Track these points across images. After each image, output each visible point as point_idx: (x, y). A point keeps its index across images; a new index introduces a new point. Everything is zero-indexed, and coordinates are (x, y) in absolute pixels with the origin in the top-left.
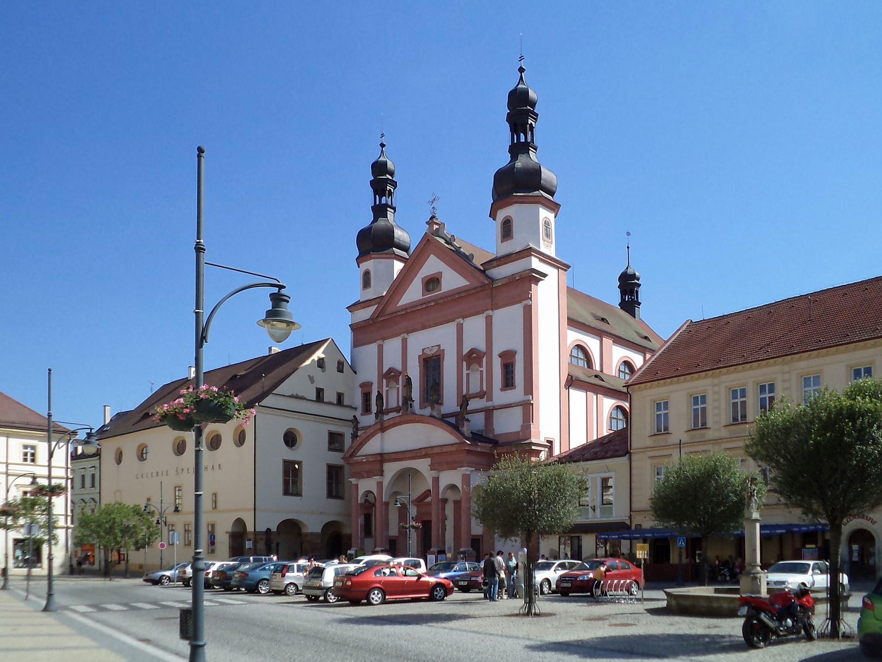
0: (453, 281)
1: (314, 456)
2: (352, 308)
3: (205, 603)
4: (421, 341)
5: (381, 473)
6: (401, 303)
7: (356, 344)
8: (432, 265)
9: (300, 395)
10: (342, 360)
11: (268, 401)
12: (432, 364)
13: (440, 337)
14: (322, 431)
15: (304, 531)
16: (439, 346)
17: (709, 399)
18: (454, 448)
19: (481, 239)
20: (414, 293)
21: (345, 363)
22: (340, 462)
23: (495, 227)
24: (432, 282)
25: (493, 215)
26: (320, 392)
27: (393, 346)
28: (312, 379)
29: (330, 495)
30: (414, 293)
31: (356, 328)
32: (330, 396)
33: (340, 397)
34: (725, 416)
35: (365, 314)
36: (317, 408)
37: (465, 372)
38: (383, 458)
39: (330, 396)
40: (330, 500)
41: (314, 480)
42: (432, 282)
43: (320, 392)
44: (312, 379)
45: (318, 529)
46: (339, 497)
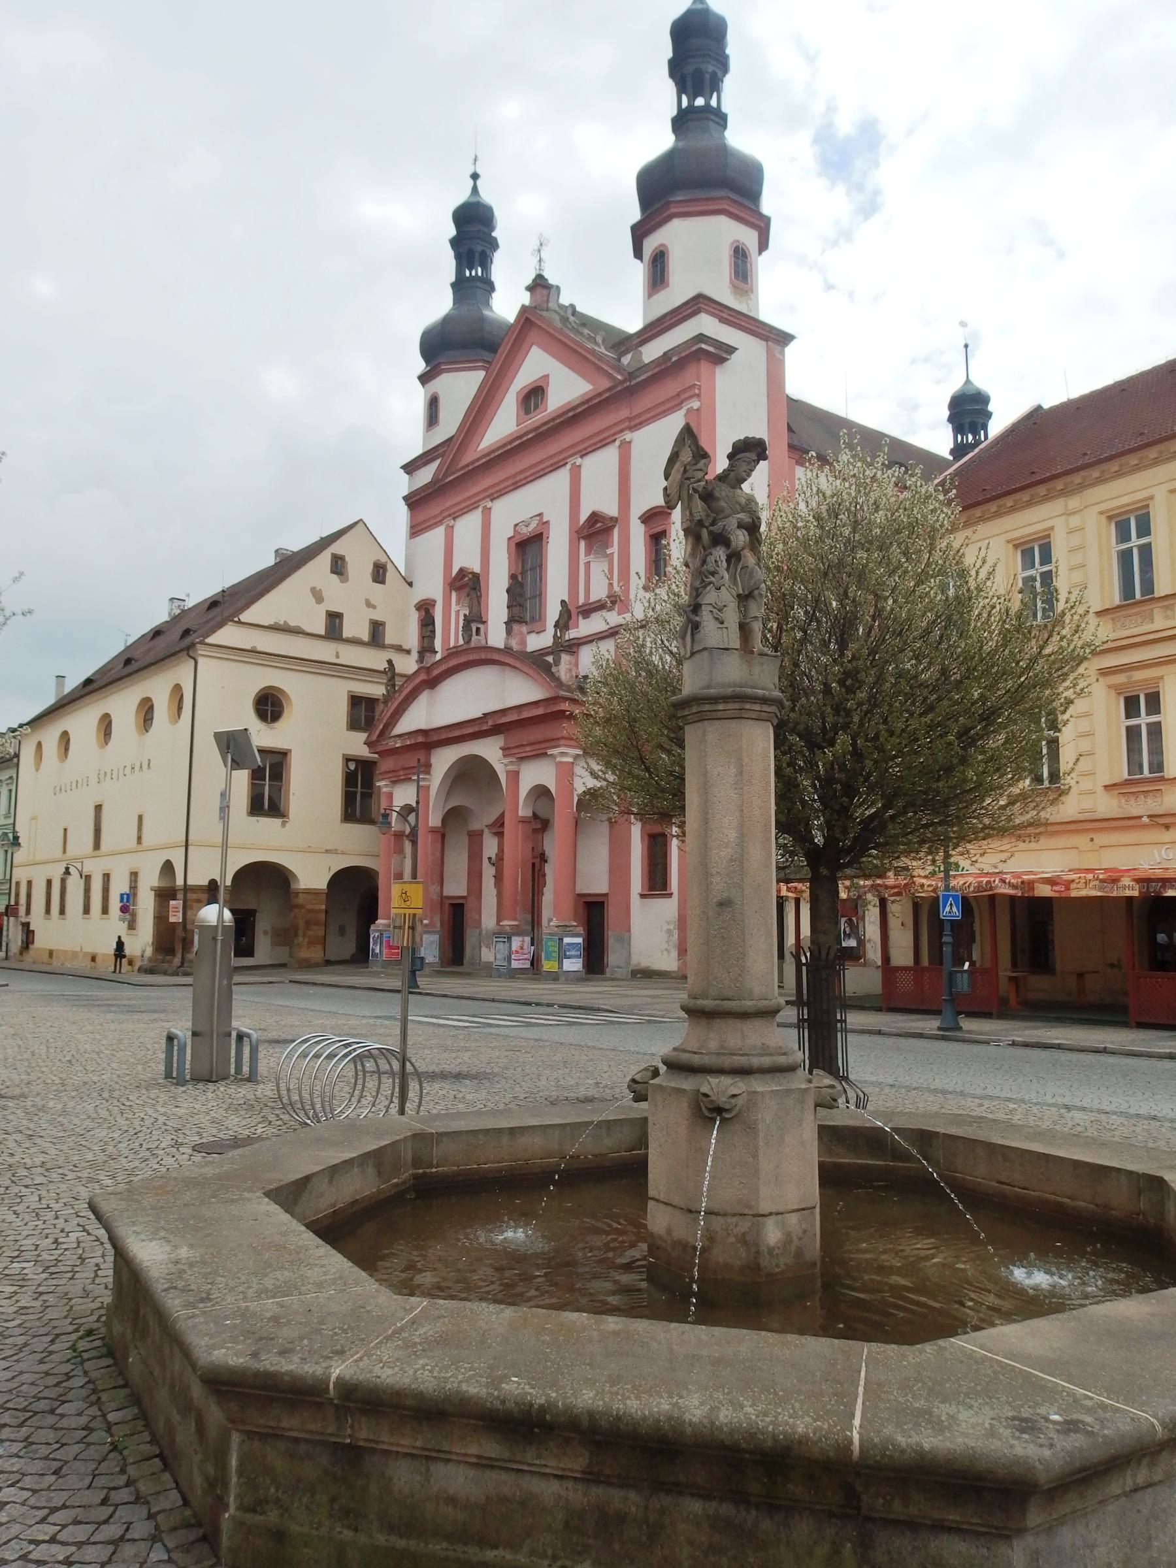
0: (567, 388)
1: (318, 741)
2: (410, 468)
3: (579, 940)
4: (512, 512)
5: (427, 768)
6: (480, 448)
7: (416, 530)
8: (537, 363)
9: (292, 624)
10: (383, 559)
11: (227, 635)
12: (528, 546)
13: (543, 500)
14: (339, 692)
15: (294, 886)
16: (540, 515)
17: (1059, 551)
18: (540, 711)
19: (617, 300)
20: (504, 423)
21: (389, 566)
22: (364, 752)
23: (638, 272)
24: (534, 395)
25: (638, 253)
26: (334, 618)
27: (468, 527)
28: (318, 596)
29: (349, 815)
30: (504, 423)
31: (414, 501)
32: (356, 626)
33: (377, 628)
34: (1103, 588)
35: (426, 475)
36: (325, 651)
37: (583, 558)
38: (430, 740)
39: (356, 626)
40: (350, 826)
41: (314, 786)
42: (534, 395)
43: (334, 618)
44: (318, 596)
45: (321, 883)
46: (366, 818)
